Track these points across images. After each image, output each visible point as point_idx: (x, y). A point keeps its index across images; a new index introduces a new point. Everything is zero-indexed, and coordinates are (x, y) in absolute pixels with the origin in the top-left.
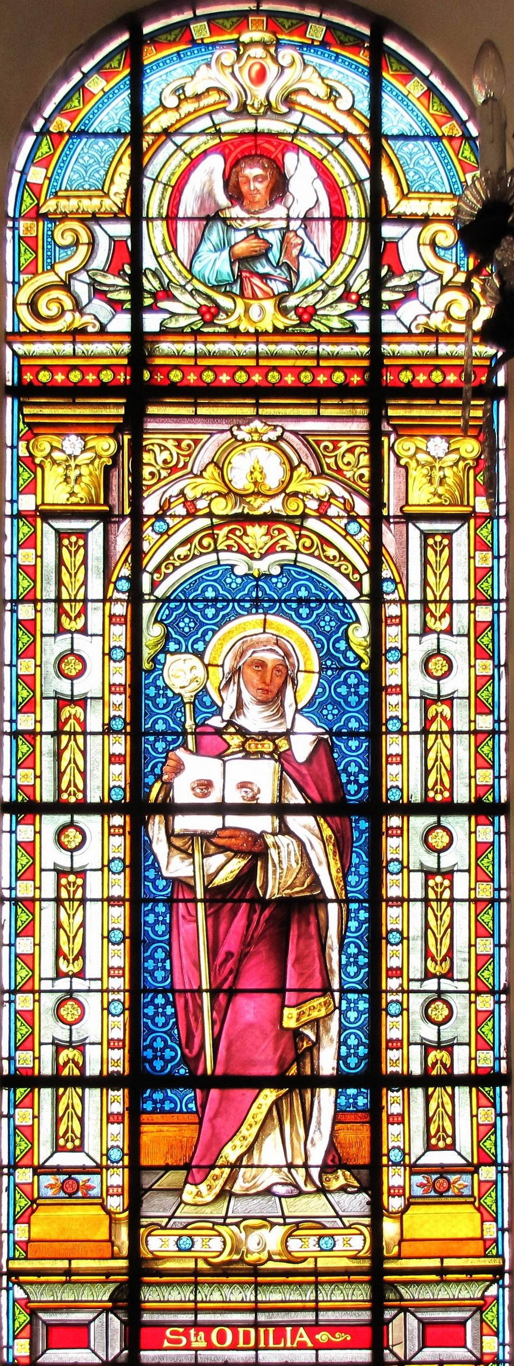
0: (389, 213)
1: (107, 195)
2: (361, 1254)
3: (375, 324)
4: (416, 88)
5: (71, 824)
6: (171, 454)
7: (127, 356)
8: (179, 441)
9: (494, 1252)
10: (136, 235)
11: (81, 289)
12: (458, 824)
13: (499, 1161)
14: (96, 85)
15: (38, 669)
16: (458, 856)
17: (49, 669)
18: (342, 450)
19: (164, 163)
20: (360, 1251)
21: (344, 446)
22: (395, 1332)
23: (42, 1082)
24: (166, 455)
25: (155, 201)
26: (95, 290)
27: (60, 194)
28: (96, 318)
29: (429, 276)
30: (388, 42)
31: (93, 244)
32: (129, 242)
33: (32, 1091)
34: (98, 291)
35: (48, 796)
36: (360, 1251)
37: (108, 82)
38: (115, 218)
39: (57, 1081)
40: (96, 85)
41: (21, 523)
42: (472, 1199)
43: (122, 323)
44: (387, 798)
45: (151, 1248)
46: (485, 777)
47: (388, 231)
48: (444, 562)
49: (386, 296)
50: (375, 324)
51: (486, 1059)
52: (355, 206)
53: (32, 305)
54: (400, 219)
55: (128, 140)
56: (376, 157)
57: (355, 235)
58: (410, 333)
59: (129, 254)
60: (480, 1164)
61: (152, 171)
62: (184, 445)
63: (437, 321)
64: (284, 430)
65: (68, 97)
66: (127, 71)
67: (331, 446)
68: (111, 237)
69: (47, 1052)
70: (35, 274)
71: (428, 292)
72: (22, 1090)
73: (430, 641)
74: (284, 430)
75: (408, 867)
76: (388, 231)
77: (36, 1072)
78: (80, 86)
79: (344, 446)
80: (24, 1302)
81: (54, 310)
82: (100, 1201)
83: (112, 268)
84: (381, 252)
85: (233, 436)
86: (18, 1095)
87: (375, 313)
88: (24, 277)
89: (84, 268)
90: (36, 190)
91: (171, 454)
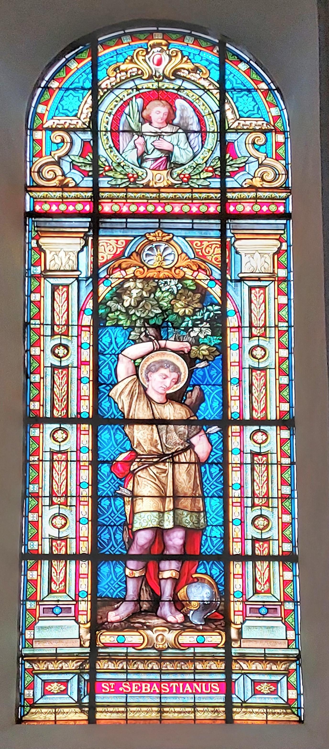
0: (229, 128)
1: (79, 119)
2: (219, 646)
3: (223, 183)
4: (243, 66)
5: (60, 429)
6: (113, 247)
7: (91, 198)
8: (117, 240)
9: (294, 647)
10: (95, 138)
11: (66, 166)
12: (271, 430)
13: (295, 600)
14: (73, 65)
15: (42, 352)
16: (271, 445)
17: (48, 351)
18: (204, 246)
19: (108, 104)
20: (219, 644)
21: (205, 244)
22: (239, 687)
23: (44, 557)
24: (110, 247)
25: (104, 121)
26: (73, 164)
27: (54, 118)
28: (73, 179)
29: (252, 159)
30: (227, 45)
31: (72, 143)
32: (92, 142)
33: (37, 562)
34: (74, 166)
35: (100, 698)
36: (219, 644)
37: (79, 63)
38: (84, 130)
39: (51, 557)
40: (73, 65)
41: (32, 281)
42: (281, 619)
43: (88, 182)
44: (231, 417)
45: (103, 641)
46: (285, 407)
47: (229, 137)
48: (261, 301)
49: (229, 168)
50: (223, 183)
51: (287, 547)
52: (212, 125)
53: (39, 172)
54: (236, 131)
55: (90, 92)
56: (222, 101)
57: (212, 140)
58: (242, 187)
59: (91, 147)
60: (285, 601)
61: (103, 108)
62: (119, 242)
63: (257, 182)
64: (173, 235)
65: (58, 71)
66: (90, 58)
67: (199, 244)
68: (82, 140)
69: (46, 544)
70: (41, 157)
71: (252, 167)
72: (32, 561)
73: (255, 341)
74: (173, 235)
75: (243, 452)
76: (229, 137)
77: (40, 552)
78: (64, 65)
79: (205, 244)
80: (31, 670)
81: (50, 176)
82: (74, 618)
83: (82, 155)
84: (225, 147)
85: (147, 238)
86: (29, 564)
87: (223, 177)
88: (35, 159)
89: (67, 154)
90: (42, 116)
91: (113, 247)
